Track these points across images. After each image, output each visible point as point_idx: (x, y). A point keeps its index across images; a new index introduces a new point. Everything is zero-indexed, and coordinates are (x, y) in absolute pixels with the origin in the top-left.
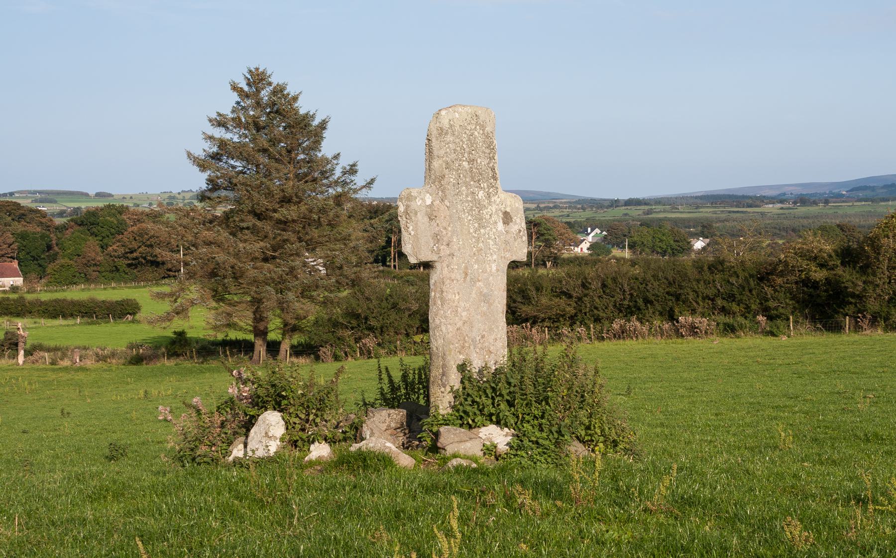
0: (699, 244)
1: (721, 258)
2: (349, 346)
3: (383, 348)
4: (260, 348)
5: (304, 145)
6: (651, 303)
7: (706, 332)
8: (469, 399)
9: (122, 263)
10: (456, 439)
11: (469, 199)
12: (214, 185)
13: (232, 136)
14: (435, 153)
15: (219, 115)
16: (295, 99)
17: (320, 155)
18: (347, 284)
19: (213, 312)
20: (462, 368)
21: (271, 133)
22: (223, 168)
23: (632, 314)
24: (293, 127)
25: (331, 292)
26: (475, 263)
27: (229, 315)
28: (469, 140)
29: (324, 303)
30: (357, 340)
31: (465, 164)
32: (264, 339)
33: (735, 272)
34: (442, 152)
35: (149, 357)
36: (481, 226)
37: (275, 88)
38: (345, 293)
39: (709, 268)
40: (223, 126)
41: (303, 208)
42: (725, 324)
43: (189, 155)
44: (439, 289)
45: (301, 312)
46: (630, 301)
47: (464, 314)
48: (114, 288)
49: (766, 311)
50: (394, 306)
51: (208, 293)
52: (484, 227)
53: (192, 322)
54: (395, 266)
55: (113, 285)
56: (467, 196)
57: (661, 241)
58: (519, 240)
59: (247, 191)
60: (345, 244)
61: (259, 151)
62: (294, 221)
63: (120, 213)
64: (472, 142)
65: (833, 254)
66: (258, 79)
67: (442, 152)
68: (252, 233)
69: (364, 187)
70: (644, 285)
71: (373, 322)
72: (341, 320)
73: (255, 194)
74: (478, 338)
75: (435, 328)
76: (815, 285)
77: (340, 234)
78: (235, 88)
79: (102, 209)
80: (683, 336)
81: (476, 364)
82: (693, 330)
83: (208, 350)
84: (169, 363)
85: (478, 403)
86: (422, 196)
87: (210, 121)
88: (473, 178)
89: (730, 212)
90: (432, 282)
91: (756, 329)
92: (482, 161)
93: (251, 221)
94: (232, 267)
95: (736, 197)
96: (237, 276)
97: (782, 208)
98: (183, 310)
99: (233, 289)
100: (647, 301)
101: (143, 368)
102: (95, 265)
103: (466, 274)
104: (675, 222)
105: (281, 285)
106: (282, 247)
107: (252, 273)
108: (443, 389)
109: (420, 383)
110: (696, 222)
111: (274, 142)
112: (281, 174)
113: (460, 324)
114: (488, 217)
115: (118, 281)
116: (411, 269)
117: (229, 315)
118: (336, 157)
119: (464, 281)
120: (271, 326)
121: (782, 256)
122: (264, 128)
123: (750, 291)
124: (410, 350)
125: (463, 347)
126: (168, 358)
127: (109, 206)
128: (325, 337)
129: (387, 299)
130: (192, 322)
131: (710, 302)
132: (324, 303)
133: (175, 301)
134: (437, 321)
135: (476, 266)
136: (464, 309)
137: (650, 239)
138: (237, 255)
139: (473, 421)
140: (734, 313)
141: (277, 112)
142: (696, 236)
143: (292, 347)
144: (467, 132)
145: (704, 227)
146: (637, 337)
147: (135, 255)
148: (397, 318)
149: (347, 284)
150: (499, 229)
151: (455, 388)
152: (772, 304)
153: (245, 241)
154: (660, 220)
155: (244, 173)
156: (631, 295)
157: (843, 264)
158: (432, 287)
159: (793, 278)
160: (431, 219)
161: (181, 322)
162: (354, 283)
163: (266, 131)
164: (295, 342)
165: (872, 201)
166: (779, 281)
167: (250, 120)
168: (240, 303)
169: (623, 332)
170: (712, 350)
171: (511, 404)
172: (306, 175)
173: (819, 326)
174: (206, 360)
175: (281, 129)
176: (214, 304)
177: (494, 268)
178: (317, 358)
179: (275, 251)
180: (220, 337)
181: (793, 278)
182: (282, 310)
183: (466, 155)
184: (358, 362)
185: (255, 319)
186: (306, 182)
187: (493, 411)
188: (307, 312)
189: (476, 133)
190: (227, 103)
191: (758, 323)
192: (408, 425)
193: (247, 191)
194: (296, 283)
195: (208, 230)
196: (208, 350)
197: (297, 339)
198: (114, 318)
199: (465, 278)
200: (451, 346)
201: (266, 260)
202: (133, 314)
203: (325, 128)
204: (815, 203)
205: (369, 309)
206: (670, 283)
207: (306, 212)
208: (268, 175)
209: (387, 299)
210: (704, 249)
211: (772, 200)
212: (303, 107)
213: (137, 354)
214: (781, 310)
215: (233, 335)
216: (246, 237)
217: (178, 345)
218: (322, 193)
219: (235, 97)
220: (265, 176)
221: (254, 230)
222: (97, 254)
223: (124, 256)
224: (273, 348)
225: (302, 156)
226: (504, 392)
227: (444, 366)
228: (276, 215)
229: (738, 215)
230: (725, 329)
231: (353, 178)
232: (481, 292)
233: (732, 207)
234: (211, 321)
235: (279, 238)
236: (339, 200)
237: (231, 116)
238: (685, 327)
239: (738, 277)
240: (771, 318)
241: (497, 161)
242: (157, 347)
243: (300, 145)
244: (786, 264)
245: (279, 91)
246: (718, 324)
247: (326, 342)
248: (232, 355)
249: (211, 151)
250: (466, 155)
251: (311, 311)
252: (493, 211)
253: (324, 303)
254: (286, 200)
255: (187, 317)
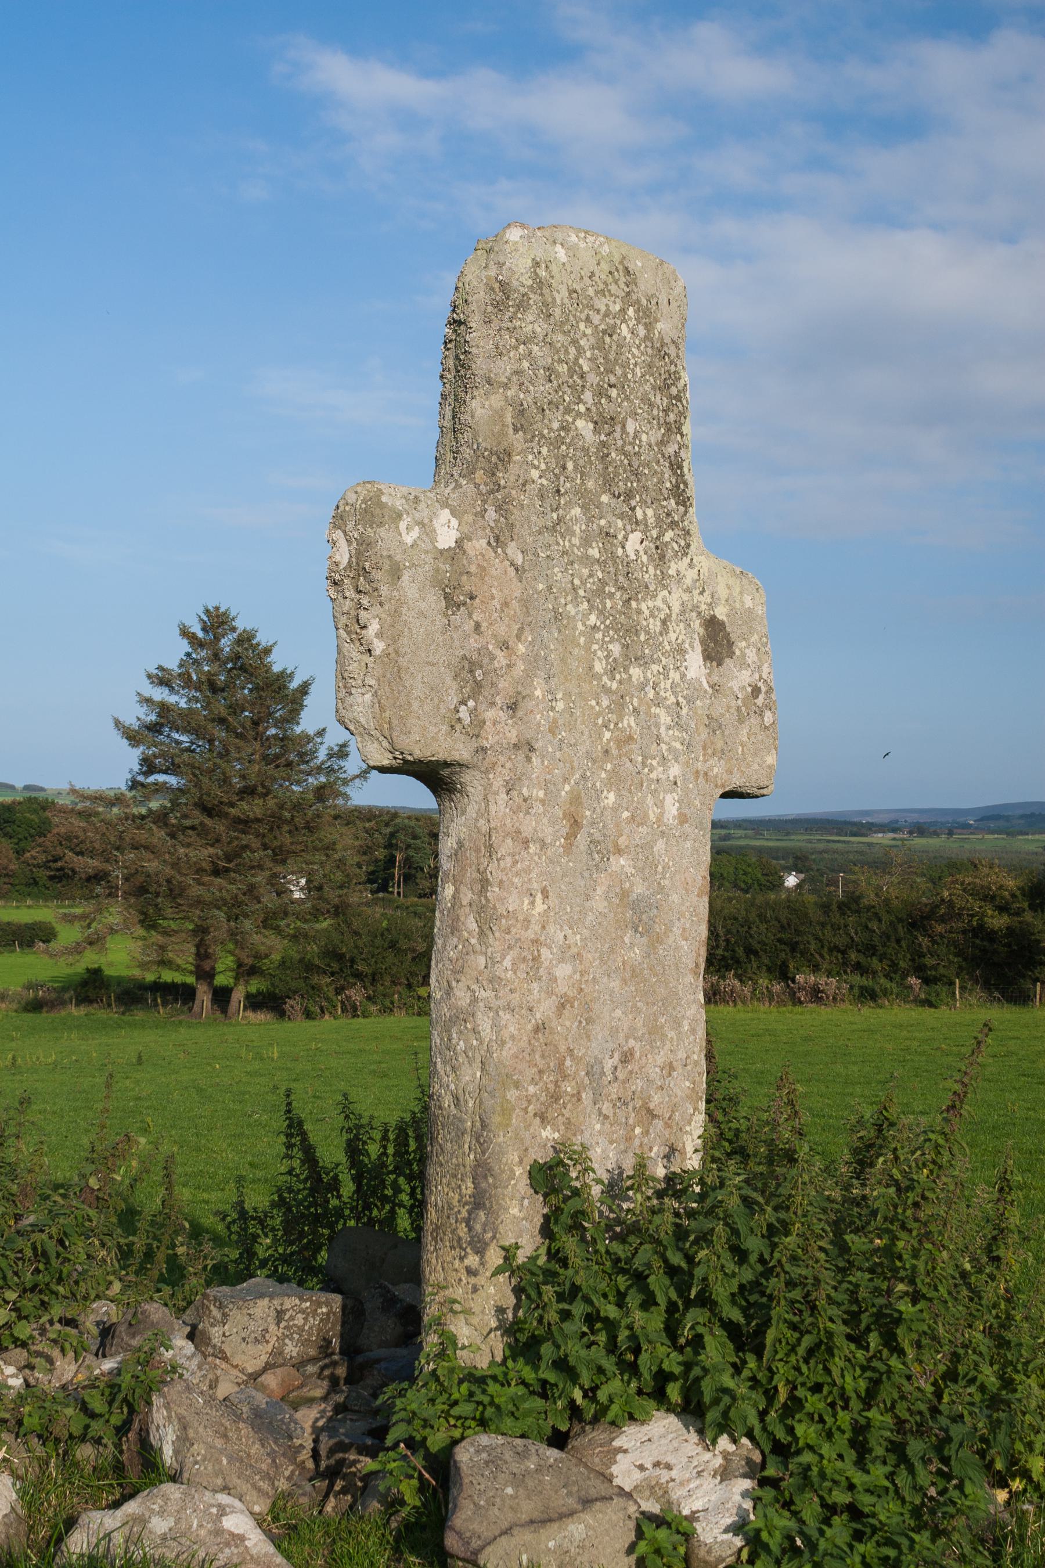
0: (791, 881)
1: (857, 893)
2: (327, 999)
3: (375, 1003)
4: (204, 997)
5: (278, 715)
6: (756, 953)
7: (834, 999)
8: (578, 1309)
9: (43, 874)
10: (528, 1509)
11: (594, 552)
12: (149, 766)
13: (179, 700)
14: (480, 365)
15: (160, 668)
16: (268, 651)
17: (298, 730)
18: (328, 912)
19: (140, 943)
20: (548, 1178)
21: (229, 698)
22: (162, 743)
23: (728, 968)
24: (263, 689)
25: (306, 921)
26: (609, 784)
27: (162, 948)
28: (600, 346)
29: (294, 938)
30: (339, 991)
31: (584, 426)
32: (210, 984)
33: (876, 914)
34: (504, 368)
35: (52, 1002)
36: (632, 656)
37: (240, 635)
38: (325, 925)
39: (839, 907)
40: (167, 685)
41: (271, 803)
42: (861, 988)
43: (117, 723)
44: (471, 874)
45: (262, 948)
46: (726, 950)
47: (563, 971)
48: (29, 907)
49: (919, 970)
50: (393, 945)
51: (136, 917)
52: (643, 661)
53: (111, 957)
54: (399, 893)
55: (29, 902)
56: (586, 542)
57: (745, 874)
58: (754, 720)
59: (195, 775)
60: (327, 856)
61: (213, 720)
62: (258, 820)
63: (44, 809)
64: (610, 361)
65: (1018, 893)
66: (217, 622)
67: (504, 368)
68: (199, 835)
69: (358, 776)
70: (746, 928)
71: (361, 967)
72: (317, 962)
73: (205, 780)
74: (608, 1064)
75: (453, 1020)
76: (991, 936)
77: (321, 840)
78: (185, 633)
79: (20, 803)
80: (801, 1003)
81: (604, 1156)
82: (816, 995)
83: (133, 995)
84: (76, 1011)
85: (611, 1326)
86: (423, 512)
87: (149, 676)
88: (608, 483)
89: (828, 841)
90: (447, 845)
91: (905, 995)
92: (642, 431)
93: (198, 817)
94: (169, 881)
95: (836, 822)
96: (175, 892)
97: (894, 839)
98: (98, 939)
99: (169, 912)
100: (750, 951)
101: (44, 1017)
102: (7, 875)
103: (576, 824)
104: (760, 851)
105: (235, 909)
106: (240, 856)
107: (196, 891)
108: (472, 1260)
109: (398, 1170)
110: (786, 853)
111: (235, 709)
112: (243, 754)
113: (545, 1009)
114: (655, 626)
115: (36, 897)
116: (420, 896)
117: (162, 948)
118: (321, 733)
119: (568, 848)
120: (220, 967)
121: (946, 894)
122: (223, 690)
123: (898, 941)
124: (413, 1007)
125: (555, 1097)
126: (77, 1005)
127: (30, 799)
128: (294, 985)
129: (382, 935)
130: (111, 957)
131: (840, 956)
132: (294, 938)
133: (89, 926)
134: (462, 997)
135: (611, 798)
136: (565, 954)
137: (732, 870)
138: (175, 865)
139: (590, 1393)
140: (874, 973)
141: (243, 669)
142: (789, 870)
143: (248, 996)
144: (596, 319)
145: (797, 858)
146: (734, 1002)
147: (59, 864)
148: (396, 961)
149: (328, 912)
150: (691, 674)
151: (521, 1258)
152: (929, 961)
153: (189, 845)
154: (741, 847)
155: (193, 751)
156: (727, 941)
157: (1031, 907)
158: (445, 864)
159: (960, 925)
160: (452, 603)
161: (95, 957)
162: (339, 910)
163: (225, 694)
164: (253, 989)
165: (1008, 834)
166: (940, 928)
167: (204, 678)
168: (176, 932)
169: (715, 994)
170: (855, 1027)
171: (746, 1340)
172: (277, 757)
173: (997, 994)
174: (129, 1010)
175: (246, 691)
176: (141, 932)
177: (672, 809)
178: (281, 1014)
179: (230, 861)
180: (150, 977)
181: (960, 925)
182: (236, 942)
183: (588, 396)
184: (338, 1022)
185: (198, 954)
186: (277, 766)
187: (673, 1363)
188: (271, 947)
189: (624, 330)
190: (173, 653)
191: (911, 987)
192: (350, 1350)
193: (195, 775)
194: (257, 906)
195: (138, 828)
196: (133, 995)
197: (255, 985)
198: (21, 945)
199: (571, 836)
200: (512, 1094)
201: (216, 872)
202: (46, 941)
203: (306, 693)
204: (936, 834)
205: (356, 947)
206: (783, 927)
207: (275, 808)
208: (225, 755)
209: (382, 935)
210: (799, 886)
211: (882, 828)
212: (278, 663)
213: (35, 998)
214: (942, 971)
215: (168, 976)
216: (189, 840)
217: (92, 988)
218: (298, 783)
219: (185, 646)
220: (220, 756)
221: (200, 830)
222: (10, 861)
223: (46, 865)
224: (222, 997)
225: (273, 731)
226: (721, 1292)
227: (482, 1171)
228: (233, 811)
229: (839, 845)
230: (862, 995)
231: (342, 764)
232: (625, 894)
233: (831, 835)
234: (137, 955)
235: (236, 843)
236: (321, 793)
237: (177, 671)
238: (804, 989)
239: (880, 921)
240: (927, 981)
241: (689, 440)
242: (64, 989)
243: (270, 714)
244: (951, 904)
245: (246, 639)
246: (852, 987)
247: (295, 992)
248: (165, 1004)
249: (148, 719)
250: (588, 396)
251: (275, 947)
252: (669, 606)
253: (295, 936)
254: (248, 792)
255: (103, 949)
